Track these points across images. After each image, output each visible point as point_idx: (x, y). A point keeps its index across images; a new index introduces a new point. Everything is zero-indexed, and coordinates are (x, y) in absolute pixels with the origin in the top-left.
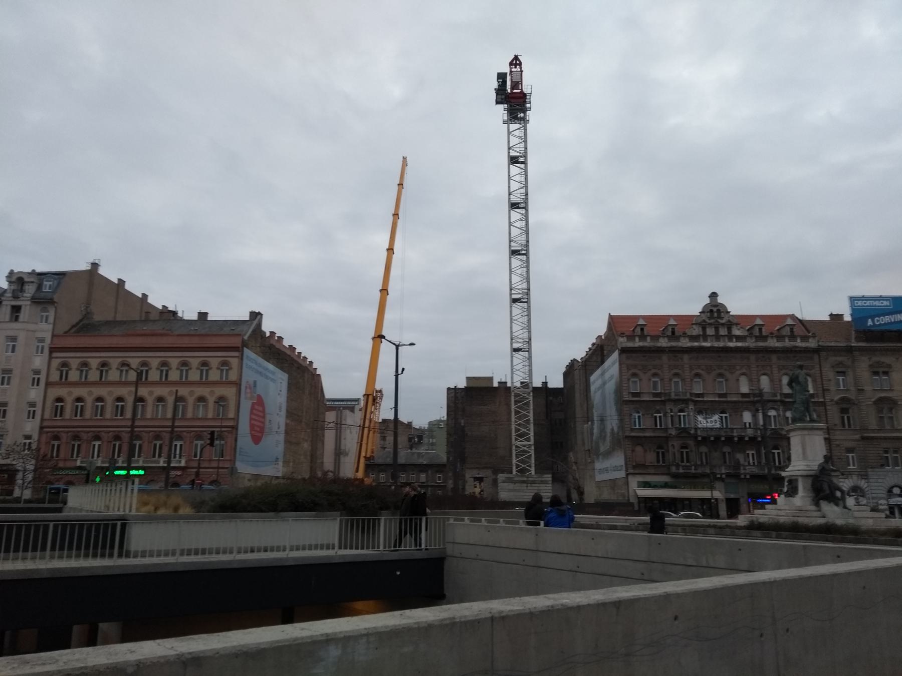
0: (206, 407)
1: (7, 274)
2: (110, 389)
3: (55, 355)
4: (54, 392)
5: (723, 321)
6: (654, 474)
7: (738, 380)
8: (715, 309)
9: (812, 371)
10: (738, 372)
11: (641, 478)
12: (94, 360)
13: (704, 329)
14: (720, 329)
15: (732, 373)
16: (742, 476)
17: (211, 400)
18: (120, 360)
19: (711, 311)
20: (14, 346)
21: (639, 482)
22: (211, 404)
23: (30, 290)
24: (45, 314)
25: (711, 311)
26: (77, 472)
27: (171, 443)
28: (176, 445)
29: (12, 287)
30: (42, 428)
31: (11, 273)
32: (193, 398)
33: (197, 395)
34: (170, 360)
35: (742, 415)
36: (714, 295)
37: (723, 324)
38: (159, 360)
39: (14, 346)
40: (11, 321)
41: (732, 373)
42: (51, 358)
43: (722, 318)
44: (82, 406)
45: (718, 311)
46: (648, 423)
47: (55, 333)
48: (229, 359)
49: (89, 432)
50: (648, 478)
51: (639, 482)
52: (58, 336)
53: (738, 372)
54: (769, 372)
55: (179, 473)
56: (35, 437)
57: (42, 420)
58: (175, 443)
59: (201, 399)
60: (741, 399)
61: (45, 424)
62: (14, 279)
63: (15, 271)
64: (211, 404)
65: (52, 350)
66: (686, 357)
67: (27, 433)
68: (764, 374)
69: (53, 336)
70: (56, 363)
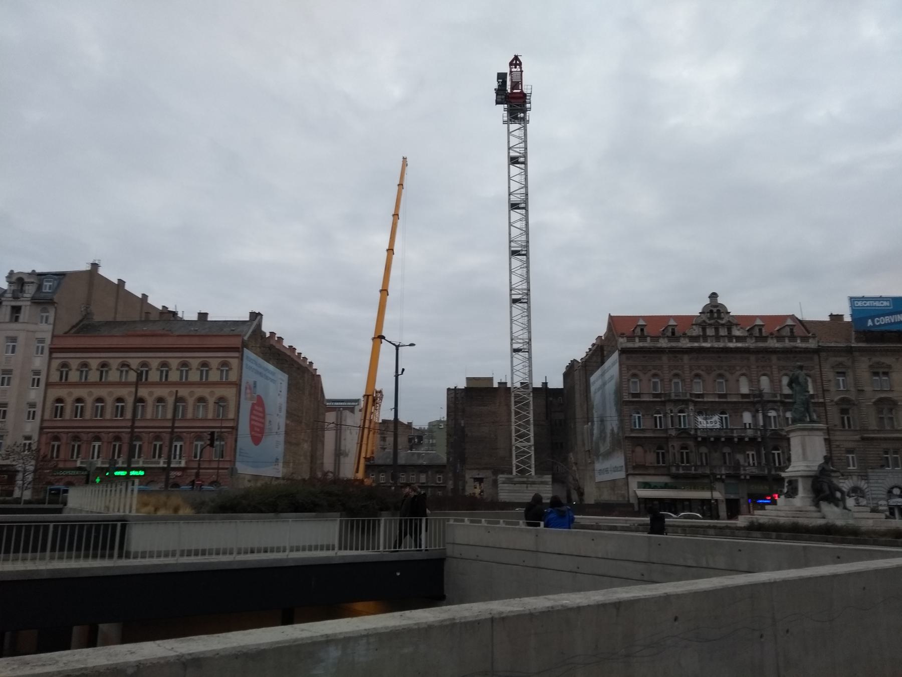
0: (206, 408)
1: (7, 274)
2: (110, 390)
3: (55, 355)
4: (54, 393)
5: (723, 322)
6: (654, 475)
7: (738, 381)
8: (715, 310)
9: (812, 372)
10: (738, 373)
11: (641, 479)
12: (94, 360)
13: (704, 329)
14: (720, 330)
15: (732, 374)
16: (742, 477)
17: (211, 401)
18: (120, 360)
19: (711, 311)
20: (14, 347)
21: (639, 483)
22: (211, 405)
23: (30, 291)
24: (45, 315)
25: (711, 311)
26: (77, 473)
27: (171, 443)
28: (176, 446)
29: (12, 288)
30: (42, 428)
31: (11, 273)
32: (193, 399)
33: (197, 395)
34: (170, 360)
35: (742, 416)
36: (714, 296)
37: (723, 325)
38: (159, 360)
39: (14, 347)
40: (11, 321)
41: (732, 374)
42: (51, 358)
43: (722, 319)
44: (82, 407)
45: (718, 311)
46: (648, 423)
47: (55, 334)
48: (229, 360)
49: (89, 433)
50: (648, 479)
51: (639, 483)
52: (58, 336)
53: (738, 373)
54: (769, 373)
55: (179, 474)
56: (35, 437)
57: (42, 420)
58: (175, 443)
59: (201, 400)
60: (741, 400)
61: (45, 424)
62: (14, 279)
63: (15, 272)
64: (211, 405)
65: (52, 350)
66: (686, 358)
67: (27, 434)
68: (764, 375)
69: (53, 336)
70: (56, 363)
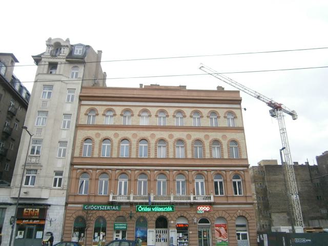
0: (221, 149)
1: (47, 40)
2: (152, 132)
3: (83, 102)
4: (83, 134)
12: (118, 108)
16: (131, 243)
17: (189, 143)
18: (141, 108)
20: (49, 93)
22: (225, 147)
23: (65, 52)
24: (75, 72)
26: (109, 208)
29: (51, 49)
30: (72, 164)
31: (50, 40)
32: (191, 141)
33: (120, 137)
34: (132, 109)
38: (88, 107)
39: (49, 93)
40: (47, 73)
42: (80, 105)
44: (39, 147)
47: (83, 85)
48: (96, 107)
49: (98, 169)
52: (86, 88)
55: (207, 209)
56: (66, 174)
57: (73, 157)
59: (216, 142)
61: (75, 161)
62: (52, 43)
63: (53, 38)
64: (225, 147)
65: (82, 98)
67: (57, 169)
69: (82, 88)
70: (84, 109)
